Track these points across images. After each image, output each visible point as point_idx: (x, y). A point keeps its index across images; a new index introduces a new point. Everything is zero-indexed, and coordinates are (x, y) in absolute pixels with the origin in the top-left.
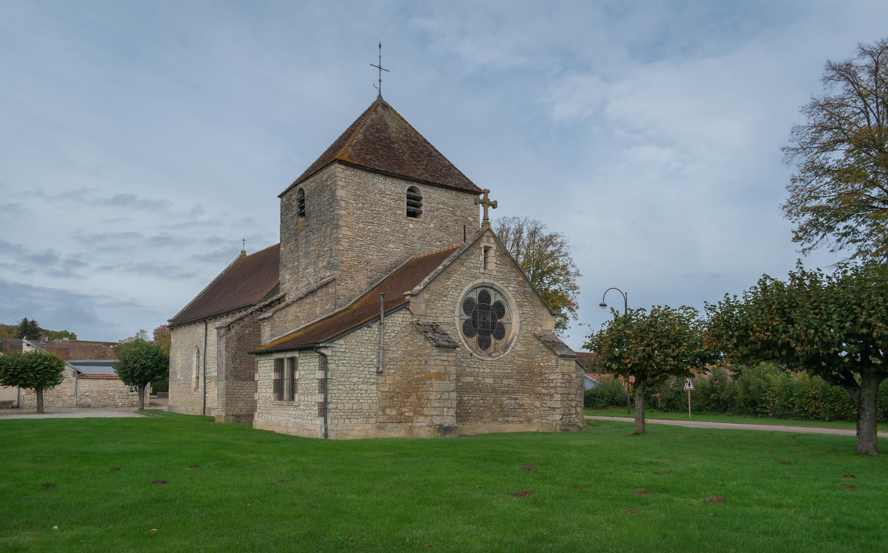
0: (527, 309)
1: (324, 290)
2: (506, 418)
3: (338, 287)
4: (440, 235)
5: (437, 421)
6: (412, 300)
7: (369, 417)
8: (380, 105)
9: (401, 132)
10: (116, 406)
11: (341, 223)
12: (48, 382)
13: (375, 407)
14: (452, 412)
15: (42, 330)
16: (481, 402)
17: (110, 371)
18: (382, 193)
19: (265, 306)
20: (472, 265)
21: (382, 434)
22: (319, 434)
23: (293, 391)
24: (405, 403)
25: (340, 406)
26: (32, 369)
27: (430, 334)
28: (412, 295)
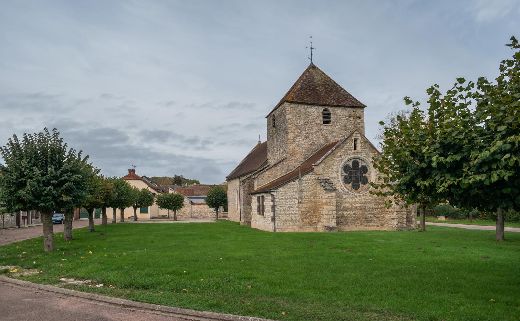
1: (281, 163)
3: (288, 162)
4: (342, 131)
5: (327, 225)
6: (315, 168)
7: (295, 222)
8: (312, 67)
9: (321, 80)
10: (208, 218)
11: (289, 131)
12: (178, 207)
13: (298, 218)
14: (334, 220)
15: (185, 179)
17: (203, 201)
18: (310, 114)
19: (260, 171)
21: (302, 231)
22: (271, 230)
23: (263, 211)
24: (313, 216)
25: (281, 218)
26: (171, 201)
27: (323, 184)
28: (315, 166)
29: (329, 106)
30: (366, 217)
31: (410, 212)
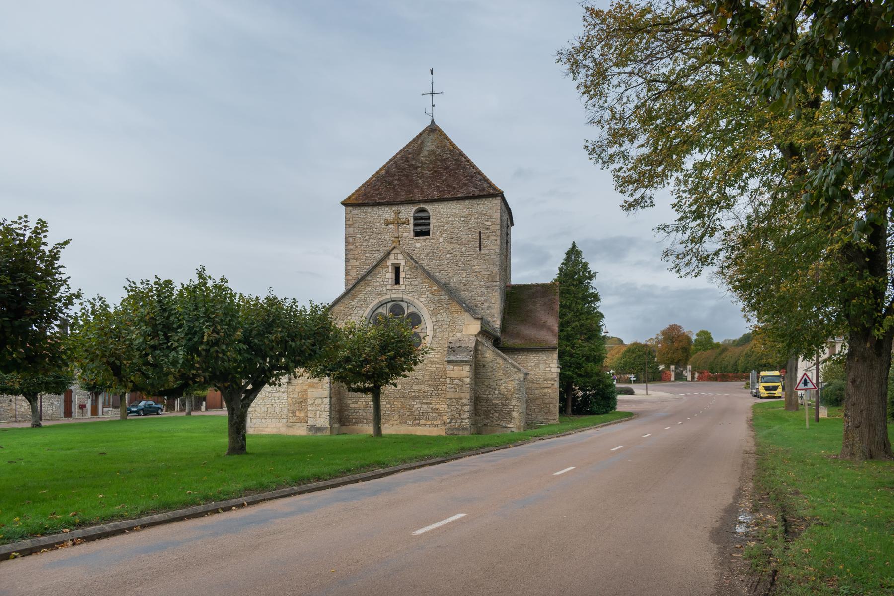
0: (444, 317)
2: (417, 422)
7: (281, 418)
8: (432, 129)
29: (425, 201)
30: (411, 410)
31: (507, 399)
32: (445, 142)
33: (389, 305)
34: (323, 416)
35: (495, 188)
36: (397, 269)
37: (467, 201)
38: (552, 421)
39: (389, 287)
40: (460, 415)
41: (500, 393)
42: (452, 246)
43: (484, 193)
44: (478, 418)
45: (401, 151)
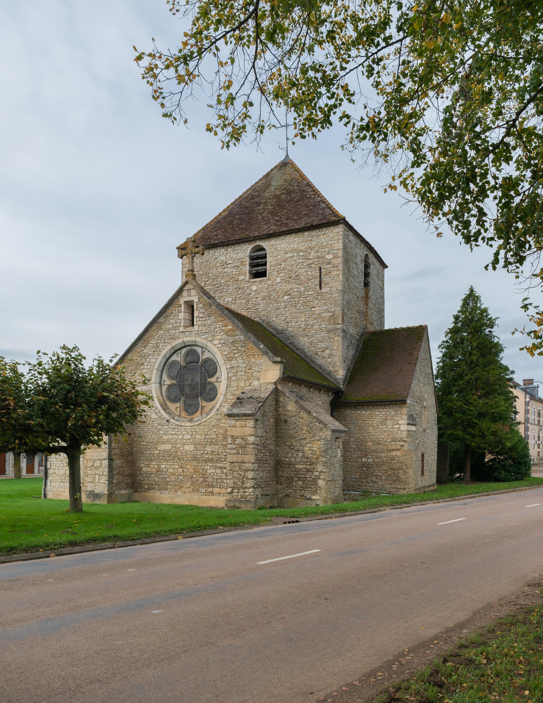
0: (239, 362)
2: (210, 489)
16: (181, 470)
18: (225, 264)
20: (171, 326)
25: (57, 471)
30: (204, 476)
31: (312, 464)
32: (296, 175)
33: (184, 351)
34: (102, 481)
35: (334, 213)
36: (190, 306)
37: (306, 233)
38: (402, 491)
39: (181, 329)
40: (243, 483)
41: (303, 456)
42: (289, 287)
43: (324, 221)
44: (279, 486)
45: (248, 190)
